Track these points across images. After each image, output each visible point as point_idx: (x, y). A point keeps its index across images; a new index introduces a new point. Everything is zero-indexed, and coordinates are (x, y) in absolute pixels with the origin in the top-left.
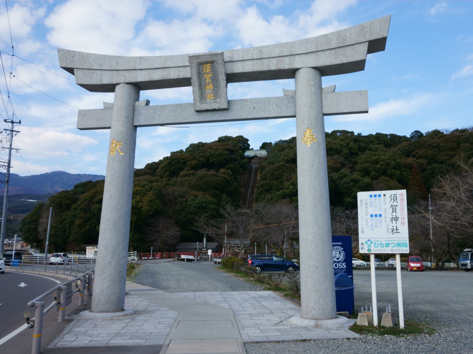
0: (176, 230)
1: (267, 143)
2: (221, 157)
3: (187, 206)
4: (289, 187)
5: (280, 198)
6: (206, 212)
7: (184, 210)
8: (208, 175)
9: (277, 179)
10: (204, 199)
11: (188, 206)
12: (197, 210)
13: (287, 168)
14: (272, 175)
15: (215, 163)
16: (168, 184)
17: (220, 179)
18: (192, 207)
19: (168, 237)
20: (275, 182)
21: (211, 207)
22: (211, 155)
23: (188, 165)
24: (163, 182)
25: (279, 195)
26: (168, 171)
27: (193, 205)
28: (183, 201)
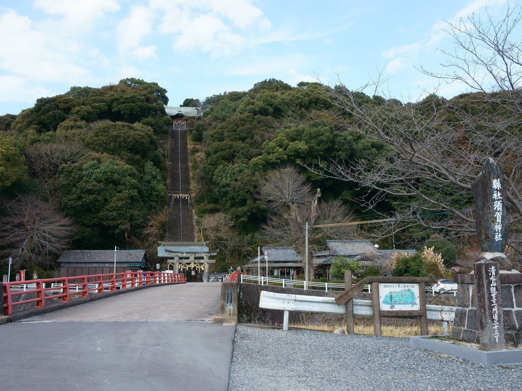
0: (62, 223)
1: (192, 99)
2: (133, 104)
3: (82, 178)
4: (273, 149)
5: (257, 170)
6: (120, 192)
7: (74, 185)
8: (117, 127)
9: (243, 139)
10: (115, 167)
11: (85, 178)
12: (102, 185)
13: (259, 122)
14: (233, 131)
15: (122, 112)
16: (39, 141)
17: (142, 133)
18: (92, 179)
19: (45, 238)
20: (240, 144)
21: (129, 182)
22: (116, 100)
23: (74, 112)
24: (29, 136)
25: (256, 165)
26: (35, 122)
27: (93, 176)
28: (72, 169)
